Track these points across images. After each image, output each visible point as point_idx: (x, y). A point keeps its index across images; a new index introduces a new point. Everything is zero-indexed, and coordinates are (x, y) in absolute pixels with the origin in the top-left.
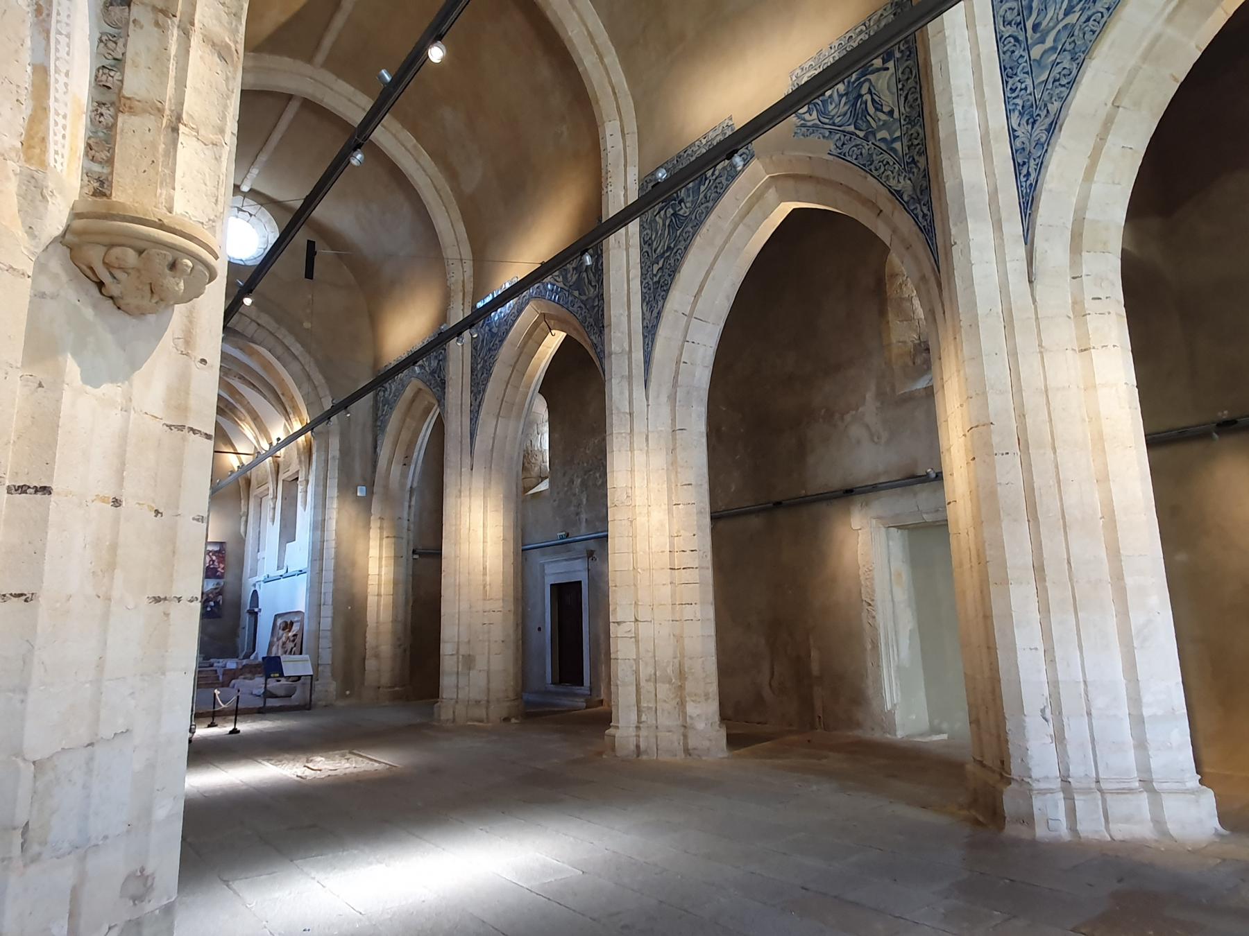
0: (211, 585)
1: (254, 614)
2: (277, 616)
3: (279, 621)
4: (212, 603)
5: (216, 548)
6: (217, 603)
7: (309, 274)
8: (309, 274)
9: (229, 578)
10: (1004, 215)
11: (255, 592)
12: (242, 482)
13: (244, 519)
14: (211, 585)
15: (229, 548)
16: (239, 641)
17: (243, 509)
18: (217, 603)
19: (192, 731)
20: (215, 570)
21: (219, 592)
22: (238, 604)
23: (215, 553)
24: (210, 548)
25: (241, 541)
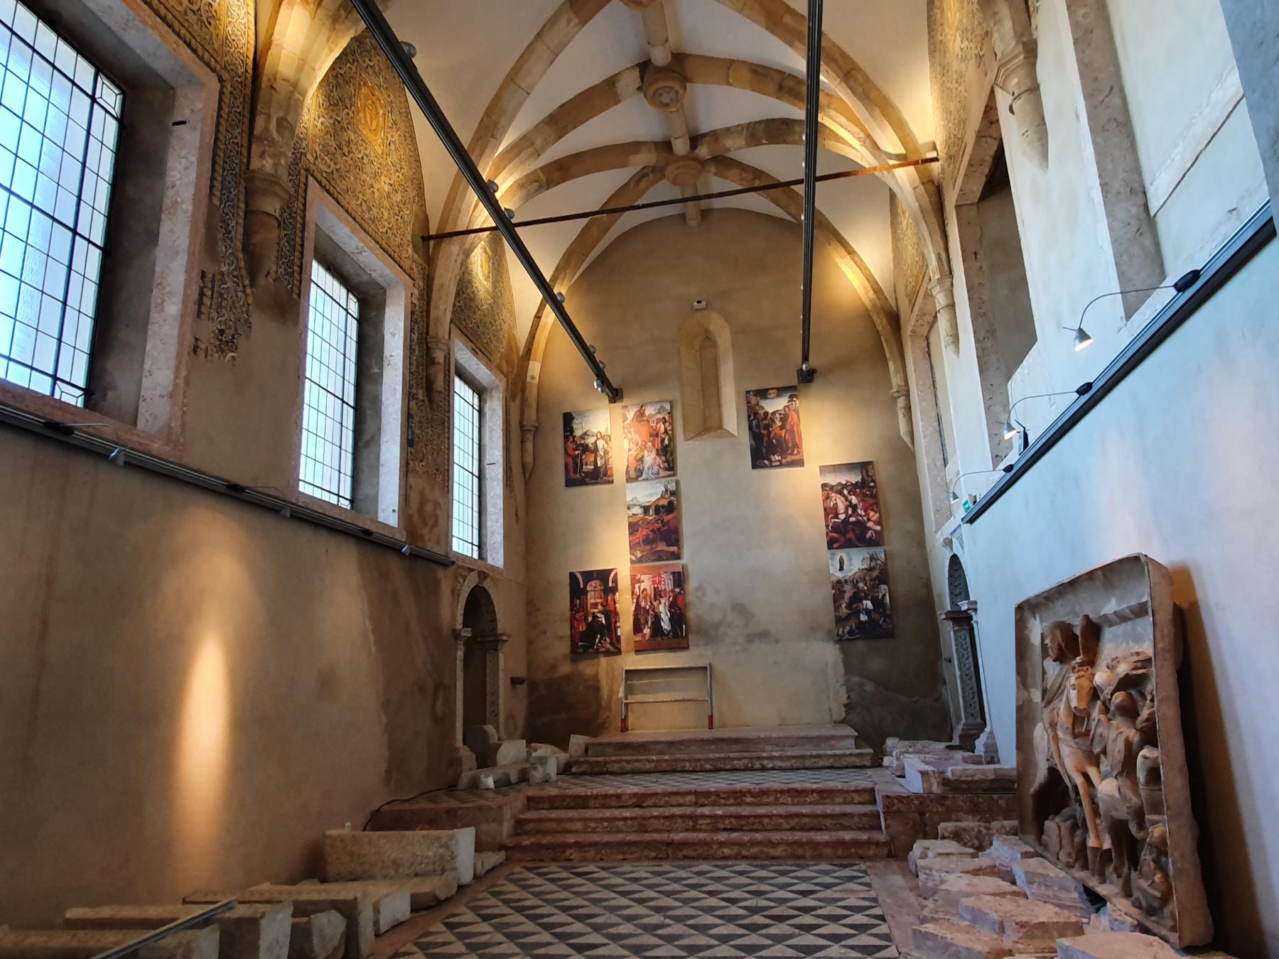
0: (856, 561)
1: (964, 620)
2: (1025, 610)
3: (1037, 629)
4: (868, 604)
5: (855, 478)
6: (878, 603)
7: (184, 123)
8: (184, 123)
9: (896, 542)
10: (81, 933)
11: (955, 560)
12: (881, 323)
13: (901, 402)
14: (856, 561)
15: (883, 474)
16: (946, 693)
17: (896, 381)
18: (878, 603)
19: (677, 483)
20: (861, 526)
21: (879, 575)
22: (927, 602)
23: (853, 488)
24: (833, 480)
25: (905, 455)
